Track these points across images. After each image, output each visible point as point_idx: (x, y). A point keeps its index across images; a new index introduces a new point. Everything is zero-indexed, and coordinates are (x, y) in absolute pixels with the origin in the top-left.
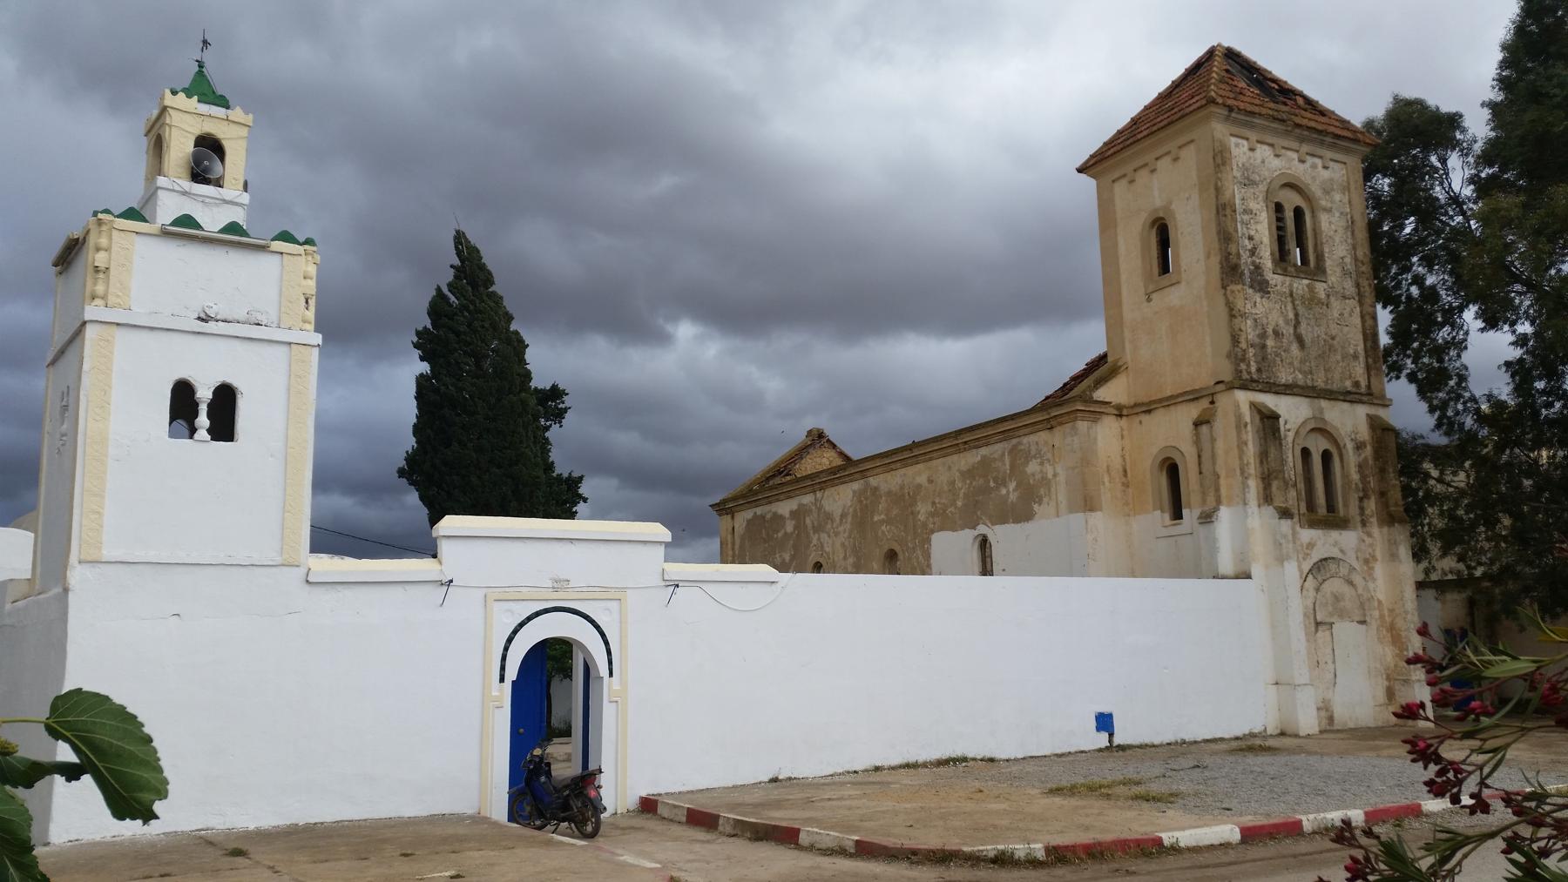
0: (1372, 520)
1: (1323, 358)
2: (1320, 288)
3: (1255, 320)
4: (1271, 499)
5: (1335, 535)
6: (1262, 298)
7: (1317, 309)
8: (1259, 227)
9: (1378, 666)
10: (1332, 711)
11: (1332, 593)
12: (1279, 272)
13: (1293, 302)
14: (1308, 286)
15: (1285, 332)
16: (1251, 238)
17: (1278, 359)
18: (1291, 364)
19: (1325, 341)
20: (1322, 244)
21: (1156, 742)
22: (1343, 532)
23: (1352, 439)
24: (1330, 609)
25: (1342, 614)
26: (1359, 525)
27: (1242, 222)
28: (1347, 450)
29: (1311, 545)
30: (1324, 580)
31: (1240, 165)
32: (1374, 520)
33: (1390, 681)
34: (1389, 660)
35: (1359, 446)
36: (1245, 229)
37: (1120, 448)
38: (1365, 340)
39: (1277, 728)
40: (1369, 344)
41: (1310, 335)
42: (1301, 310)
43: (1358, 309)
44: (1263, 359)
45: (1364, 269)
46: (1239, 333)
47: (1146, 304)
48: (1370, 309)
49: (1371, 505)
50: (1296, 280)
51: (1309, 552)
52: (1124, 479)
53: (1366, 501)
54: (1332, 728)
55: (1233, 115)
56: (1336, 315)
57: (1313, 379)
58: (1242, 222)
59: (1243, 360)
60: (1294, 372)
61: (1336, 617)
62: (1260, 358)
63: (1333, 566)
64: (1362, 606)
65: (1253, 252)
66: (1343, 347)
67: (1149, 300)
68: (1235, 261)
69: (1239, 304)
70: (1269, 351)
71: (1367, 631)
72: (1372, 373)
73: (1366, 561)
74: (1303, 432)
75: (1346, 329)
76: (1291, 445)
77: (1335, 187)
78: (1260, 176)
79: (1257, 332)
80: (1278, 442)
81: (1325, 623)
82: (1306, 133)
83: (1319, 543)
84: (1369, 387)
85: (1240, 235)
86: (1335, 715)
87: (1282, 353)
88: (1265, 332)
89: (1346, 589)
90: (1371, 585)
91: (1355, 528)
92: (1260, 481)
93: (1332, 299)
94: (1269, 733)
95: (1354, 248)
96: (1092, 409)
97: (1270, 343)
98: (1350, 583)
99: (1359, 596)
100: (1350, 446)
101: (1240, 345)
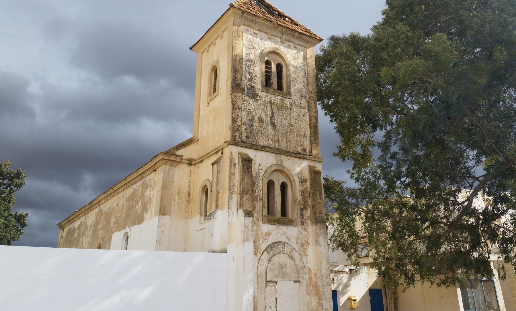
3: (248, 112)
6: (253, 102)
11: (279, 263)
12: (265, 91)
18: (267, 136)
19: (288, 127)
22: (288, 227)
23: (299, 177)
24: (276, 272)
25: (284, 276)
26: (299, 224)
27: (246, 65)
29: (268, 234)
30: (274, 255)
31: (248, 39)
42: (275, 110)
43: (308, 114)
44: (250, 132)
55: (245, 15)
57: (279, 145)
60: (268, 140)
69: (239, 103)
70: (255, 128)
79: (249, 118)
83: (274, 233)
88: (254, 119)
90: (304, 259)
91: (297, 225)
97: (256, 124)
98: (291, 257)
100: (297, 181)
101: (237, 123)
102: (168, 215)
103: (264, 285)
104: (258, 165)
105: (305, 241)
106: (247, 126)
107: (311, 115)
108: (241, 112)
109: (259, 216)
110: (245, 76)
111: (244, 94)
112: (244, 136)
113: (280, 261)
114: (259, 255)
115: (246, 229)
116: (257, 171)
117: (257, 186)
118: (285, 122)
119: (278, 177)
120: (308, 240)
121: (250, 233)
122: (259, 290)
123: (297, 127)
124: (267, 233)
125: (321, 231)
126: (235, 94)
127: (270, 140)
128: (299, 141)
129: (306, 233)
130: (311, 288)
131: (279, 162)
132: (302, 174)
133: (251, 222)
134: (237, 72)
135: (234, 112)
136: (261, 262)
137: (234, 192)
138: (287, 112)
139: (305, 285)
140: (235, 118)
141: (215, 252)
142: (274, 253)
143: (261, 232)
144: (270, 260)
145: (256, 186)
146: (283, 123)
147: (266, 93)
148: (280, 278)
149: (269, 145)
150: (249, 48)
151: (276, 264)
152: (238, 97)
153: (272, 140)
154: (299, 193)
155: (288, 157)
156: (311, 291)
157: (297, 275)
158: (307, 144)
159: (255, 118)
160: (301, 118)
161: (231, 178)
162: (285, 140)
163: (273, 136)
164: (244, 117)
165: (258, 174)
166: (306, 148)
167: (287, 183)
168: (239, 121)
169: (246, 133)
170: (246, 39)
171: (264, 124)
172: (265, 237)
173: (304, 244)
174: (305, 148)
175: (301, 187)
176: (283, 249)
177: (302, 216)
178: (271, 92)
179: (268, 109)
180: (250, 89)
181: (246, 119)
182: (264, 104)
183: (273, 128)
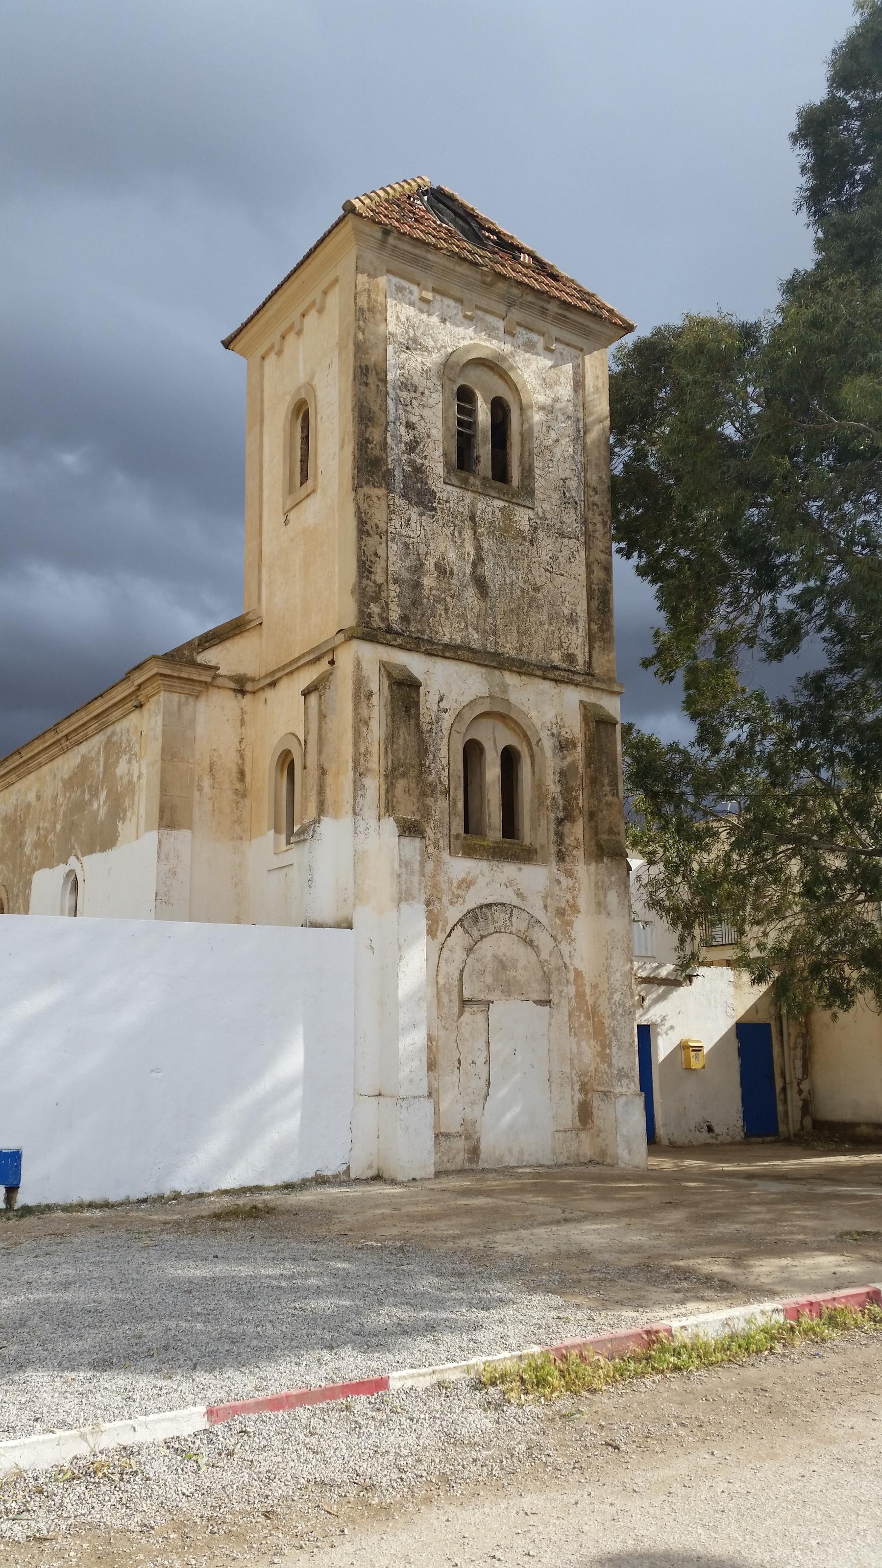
0: (575, 852)
2: (523, 518)
3: (406, 546)
4: (393, 807)
5: (509, 870)
6: (421, 515)
7: (514, 545)
8: (426, 413)
9: (567, 1069)
10: (478, 1140)
11: (495, 957)
12: (454, 481)
13: (474, 529)
14: (502, 510)
16: (410, 426)
17: (440, 607)
18: (463, 616)
19: (523, 590)
20: (531, 454)
21: (113, 1198)
22: (522, 866)
23: (553, 735)
24: (489, 979)
25: (509, 988)
26: (553, 858)
27: (398, 400)
28: (542, 749)
29: (467, 884)
30: (482, 937)
31: (403, 319)
32: (579, 853)
33: (586, 1095)
34: (586, 1060)
35: (564, 746)
36: (401, 411)
37: (238, 740)
38: (590, 597)
39: (370, 1167)
40: (595, 603)
41: (498, 581)
43: (583, 554)
44: (413, 604)
45: (596, 498)
46: (373, 558)
47: (283, 528)
48: (602, 557)
49: (577, 831)
50: (482, 497)
51: (460, 892)
52: (238, 786)
53: (568, 824)
54: (474, 1166)
56: (545, 557)
57: (497, 643)
58: (398, 400)
59: (376, 599)
60: (466, 627)
61: (498, 992)
62: (408, 602)
63: (500, 917)
64: (546, 978)
65: (412, 447)
66: (552, 605)
67: (286, 522)
68: (377, 452)
69: (379, 516)
70: (426, 592)
71: (551, 1016)
72: (597, 645)
73: (561, 913)
74: (469, 716)
75: (559, 580)
76: (446, 733)
77: (562, 379)
78: (435, 342)
79: (408, 563)
80: (412, 722)
81: (478, 1002)
82: (516, 291)
83: (481, 882)
84: (589, 664)
85: (391, 418)
86: (483, 1146)
88: (422, 565)
89: (522, 953)
90: (564, 947)
91: (545, 862)
92: (382, 778)
93: (541, 534)
94: (353, 1176)
95: (585, 469)
97: (428, 581)
98: (529, 943)
99: (542, 964)
100: (548, 744)
101: (373, 577)
102: (184, 828)
104: (437, 698)
105: (567, 902)
106: (405, 587)
108: (384, 545)
109: (439, 835)
112: (395, 614)
113: (500, 954)
115: (404, 870)
116: (433, 714)
117: (434, 755)
118: (514, 577)
121: (416, 879)
123: (549, 592)
124: (464, 880)
126: (366, 489)
127: (470, 630)
128: (556, 634)
129: (571, 882)
130: (582, 1019)
132: (561, 724)
135: (363, 543)
139: (565, 1009)
140: (368, 563)
142: (482, 933)
143: (446, 878)
144: (471, 949)
145: (431, 757)
146: (508, 581)
147: (459, 490)
150: (407, 348)
152: (375, 500)
154: (552, 777)
155: (523, 677)
156: (581, 1026)
158: (580, 641)
159: (427, 563)
160: (561, 566)
162: (514, 629)
164: (395, 558)
165: (437, 722)
166: (577, 652)
167: (519, 748)
168: (379, 571)
170: (398, 317)
171: (453, 581)
173: (564, 909)
174: (573, 654)
176: (508, 923)
177: (561, 838)
181: (399, 565)
183: (481, 593)
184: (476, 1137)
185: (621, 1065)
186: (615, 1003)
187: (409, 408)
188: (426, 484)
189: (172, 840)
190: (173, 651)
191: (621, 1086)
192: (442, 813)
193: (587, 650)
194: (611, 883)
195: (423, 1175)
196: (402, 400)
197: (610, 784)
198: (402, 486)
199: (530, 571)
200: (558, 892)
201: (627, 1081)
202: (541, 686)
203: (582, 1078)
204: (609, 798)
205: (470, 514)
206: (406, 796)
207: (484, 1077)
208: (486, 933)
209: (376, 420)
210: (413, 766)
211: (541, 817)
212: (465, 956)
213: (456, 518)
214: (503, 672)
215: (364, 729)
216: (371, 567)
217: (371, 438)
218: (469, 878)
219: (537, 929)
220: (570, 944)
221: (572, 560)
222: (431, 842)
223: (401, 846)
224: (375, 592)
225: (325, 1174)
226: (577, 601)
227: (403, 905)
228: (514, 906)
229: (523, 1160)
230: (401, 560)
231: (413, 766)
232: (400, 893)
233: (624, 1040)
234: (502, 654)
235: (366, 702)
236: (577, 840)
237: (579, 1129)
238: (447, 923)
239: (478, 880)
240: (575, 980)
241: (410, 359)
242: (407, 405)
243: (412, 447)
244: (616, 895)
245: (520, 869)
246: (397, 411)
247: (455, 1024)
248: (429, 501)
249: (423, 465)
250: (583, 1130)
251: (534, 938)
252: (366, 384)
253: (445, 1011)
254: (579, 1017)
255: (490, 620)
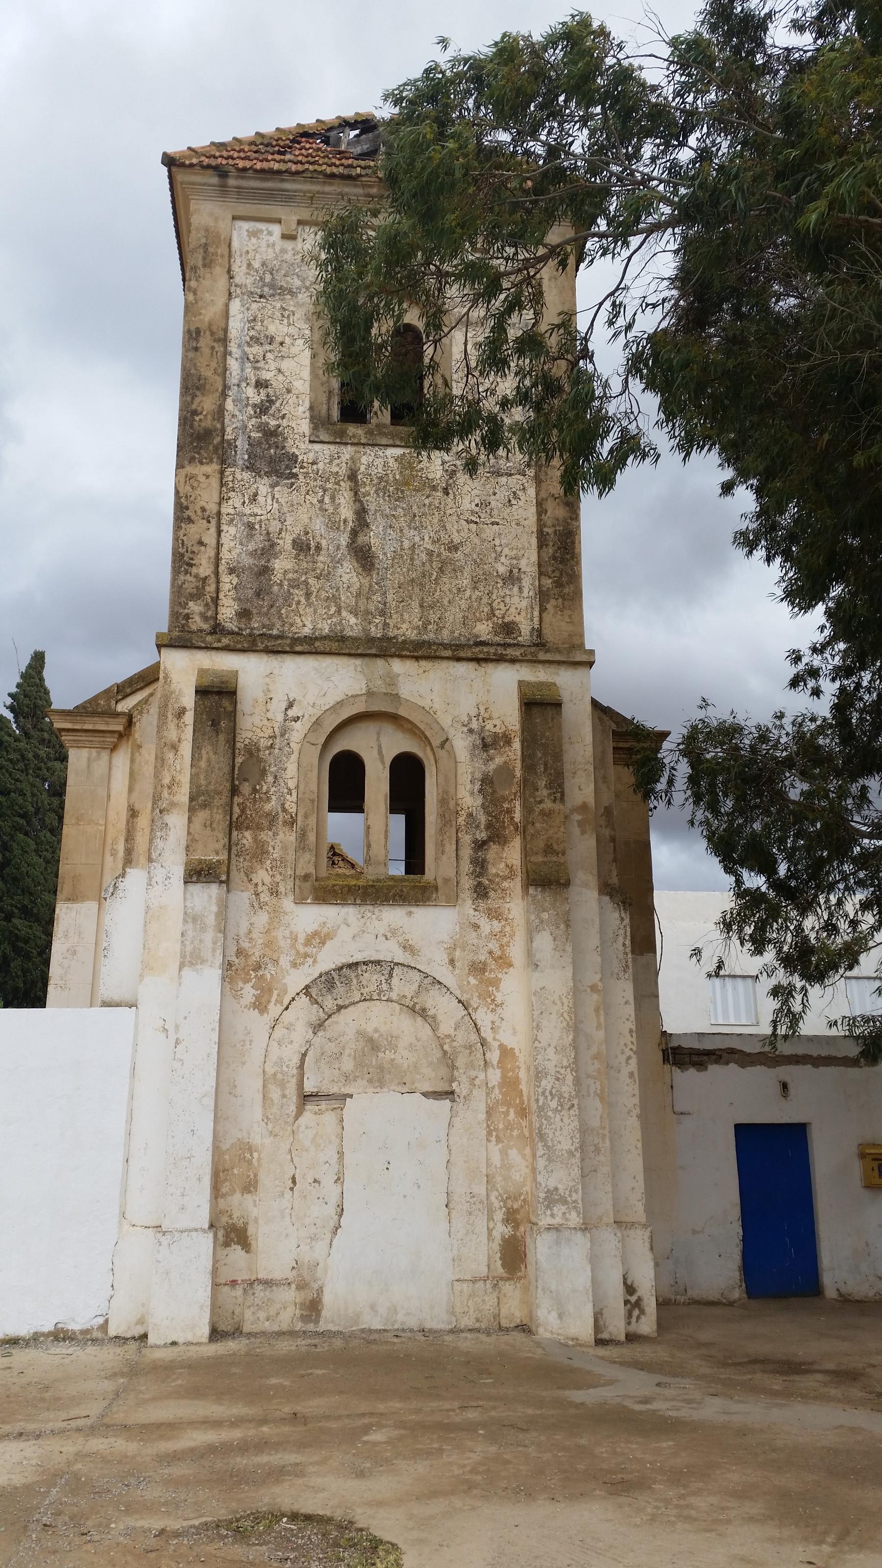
0: (505, 884)
1: (422, 586)
3: (251, 526)
6: (273, 486)
8: (285, 365)
9: (481, 1190)
10: (320, 1290)
11: (360, 1034)
12: (324, 436)
15: (324, 543)
17: (298, 594)
18: (335, 598)
19: (430, 553)
22: (414, 909)
23: (471, 731)
24: (348, 1065)
26: (467, 896)
27: (245, 358)
29: (319, 938)
30: (340, 1008)
31: (256, 265)
33: (516, 1227)
42: (372, 502)
43: (532, 492)
44: (258, 594)
50: (368, 450)
51: (309, 950)
53: (494, 848)
54: (311, 1327)
55: (232, 182)
57: (386, 625)
60: (339, 611)
62: (250, 593)
63: (371, 979)
64: (448, 1061)
69: (207, 497)
70: (277, 577)
75: (489, 532)
79: (251, 547)
81: (328, 1097)
83: (345, 934)
86: (327, 1299)
87: (311, 581)
88: (273, 545)
90: (483, 1017)
91: (453, 900)
96: (90, 727)
97: (281, 565)
98: (419, 1012)
100: (461, 745)
101: (194, 570)
102: (89, 899)
103: (293, 1108)
104: (284, 705)
105: (491, 953)
106: (244, 577)
107: (543, 495)
108: (213, 530)
109: (278, 878)
110: (240, 401)
111: (234, 465)
112: (228, 611)
113: (370, 1029)
114: (274, 1010)
115: (190, 926)
116: (276, 725)
117: (276, 777)
118: (417, 539)
119: (378, 739)
120: (503, 951)
121: (209, 937)
122: (270, 1126)
123: (473, 549)
124: (316, 934)
125: (545, 916)
126: (190, 469)
127: (344, 613)
128: (485, 600)
129: (497, 925)
130: (512, 1115)
131: (380, 686)
132: (486, 715)
133: (214, 901)
134: (198, 389)
135: (181, 533)
136: (279, 1032)
137: (173, 804)
138: (427, 502)
139: (479, 1103)
140: (187, 556)
141: (118, 1005)
142: (340, 1002)
143: (287, 933)
145: (270, 779)
146: (406, 544)
147: (332, 447)
148: (365, 1083)
149: (342, 631)
150: (261, 297)
151: (351, 1033)
152: (202, 479)
153: (354, 612)
154: (469, 786)
155: (423, 663)
156: (509, 1127)
157: (444, 1071)
158: (524, 603)
159: (281, 542)
160: (495, 512)
161: (163, 760)
162: (415, 604)
163: (358, 595)
164: (232, 544)
165: (282, 735)
166: (518, 619)
167: (421, 754)
168: (204, 562)
169: (238, 599)
170: (249, 265)
171: (321, 558)
172: (302, 949)
173: (485, 964)
174: (513, 623)
175: (479, 764)
176: (385, 986)
177: (482, 867)
178: (354, 436)
179: (342, 501)
180: (260, 443)
181: (237, 551)
182: (321, 487)
183: (363, 566)
184: (316, 1286)
185: (552, 1184)
186: (543, 1093)
187: (261, 364)
188: (284, 447)
189: (73, 914)
190: (85, 702)
191: (552, 1216)
192: (285, 848)
193: (536, 613)
194: (542, 922)
195: (190, 1337)
196: (251, 357)
197: (549, 786)
198: (246, 457)
199: (444, 526)
200: (475, 941)
201: (564, 1208)
202: (452, 671)
203: (509, 1202)
204: (548, 805)
205: (349, 472)
206: (208, 831)
207: (334, 1200)
208: (347, 1003)
209: (207, 387)
210: (219, 793)
211: (446, 842)
212: (310, 1035)
213: (328, 480)
214: (389, 659)
215: (171, 755)
216: (192, 559)
217: (199, 409)
218: (325, 930)
219: (435, 992)
220: (493, 1011)
221: (514, 502)
222: (265, 888)
223: (188, 895)
224: (197, 587)
225: (70, 1328)
226: (520, 554)
227: (187, 972)
228: (397, 964)
229: (396, 1321)
230: (241, 544)
231: (219, 793)
232: (183, 956)
233: (559, 1147)
234: (394, 638)
235: (175, 721)
236: (510, 868)
237: (502, 1279)
238: (285, 992)
239: (339, 932)
240: (499, 1062)
241: (264, 308)
242: (258, 362)
243: (263, 409)
244: (550, 938)
245: (410, 913)
246: (242, 370)
247: (289, 1129)
248: (287, 467)
249: (279, 426)
250: (508, 1279)
251: (428, 1006)
252: (196, 349)
253: (274, 1110)
254: (507, 1113)
255: (377, 597)
